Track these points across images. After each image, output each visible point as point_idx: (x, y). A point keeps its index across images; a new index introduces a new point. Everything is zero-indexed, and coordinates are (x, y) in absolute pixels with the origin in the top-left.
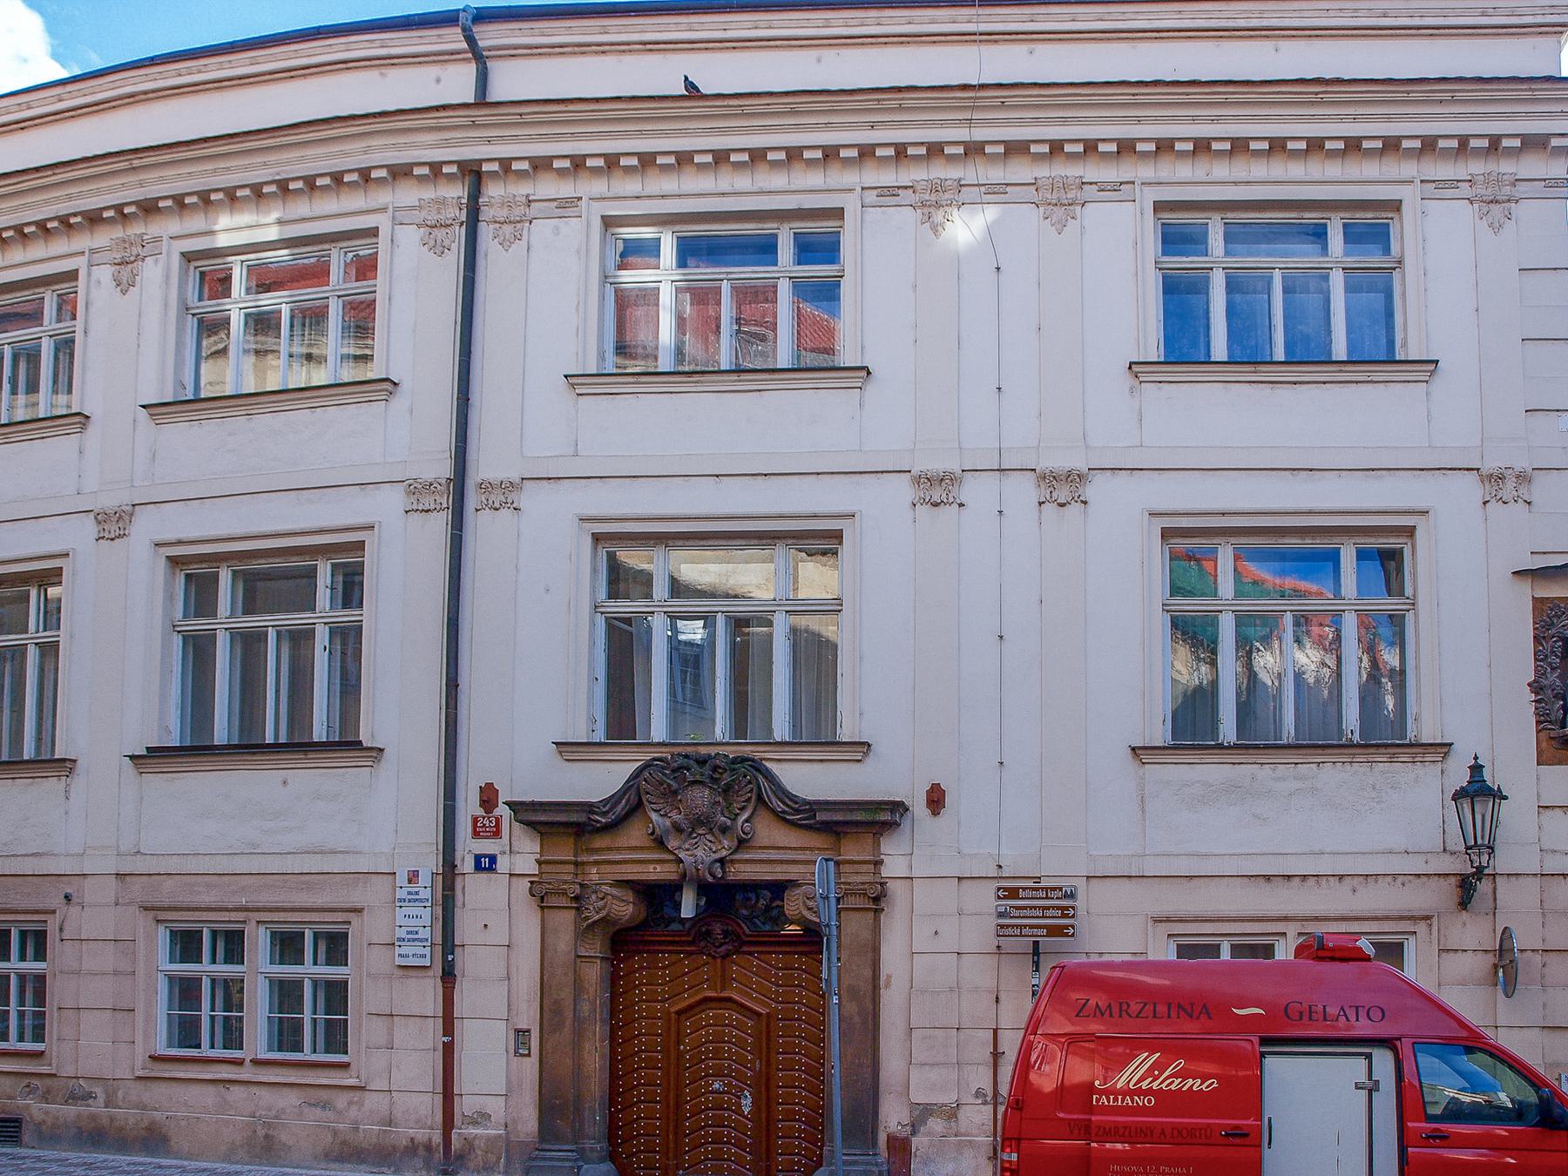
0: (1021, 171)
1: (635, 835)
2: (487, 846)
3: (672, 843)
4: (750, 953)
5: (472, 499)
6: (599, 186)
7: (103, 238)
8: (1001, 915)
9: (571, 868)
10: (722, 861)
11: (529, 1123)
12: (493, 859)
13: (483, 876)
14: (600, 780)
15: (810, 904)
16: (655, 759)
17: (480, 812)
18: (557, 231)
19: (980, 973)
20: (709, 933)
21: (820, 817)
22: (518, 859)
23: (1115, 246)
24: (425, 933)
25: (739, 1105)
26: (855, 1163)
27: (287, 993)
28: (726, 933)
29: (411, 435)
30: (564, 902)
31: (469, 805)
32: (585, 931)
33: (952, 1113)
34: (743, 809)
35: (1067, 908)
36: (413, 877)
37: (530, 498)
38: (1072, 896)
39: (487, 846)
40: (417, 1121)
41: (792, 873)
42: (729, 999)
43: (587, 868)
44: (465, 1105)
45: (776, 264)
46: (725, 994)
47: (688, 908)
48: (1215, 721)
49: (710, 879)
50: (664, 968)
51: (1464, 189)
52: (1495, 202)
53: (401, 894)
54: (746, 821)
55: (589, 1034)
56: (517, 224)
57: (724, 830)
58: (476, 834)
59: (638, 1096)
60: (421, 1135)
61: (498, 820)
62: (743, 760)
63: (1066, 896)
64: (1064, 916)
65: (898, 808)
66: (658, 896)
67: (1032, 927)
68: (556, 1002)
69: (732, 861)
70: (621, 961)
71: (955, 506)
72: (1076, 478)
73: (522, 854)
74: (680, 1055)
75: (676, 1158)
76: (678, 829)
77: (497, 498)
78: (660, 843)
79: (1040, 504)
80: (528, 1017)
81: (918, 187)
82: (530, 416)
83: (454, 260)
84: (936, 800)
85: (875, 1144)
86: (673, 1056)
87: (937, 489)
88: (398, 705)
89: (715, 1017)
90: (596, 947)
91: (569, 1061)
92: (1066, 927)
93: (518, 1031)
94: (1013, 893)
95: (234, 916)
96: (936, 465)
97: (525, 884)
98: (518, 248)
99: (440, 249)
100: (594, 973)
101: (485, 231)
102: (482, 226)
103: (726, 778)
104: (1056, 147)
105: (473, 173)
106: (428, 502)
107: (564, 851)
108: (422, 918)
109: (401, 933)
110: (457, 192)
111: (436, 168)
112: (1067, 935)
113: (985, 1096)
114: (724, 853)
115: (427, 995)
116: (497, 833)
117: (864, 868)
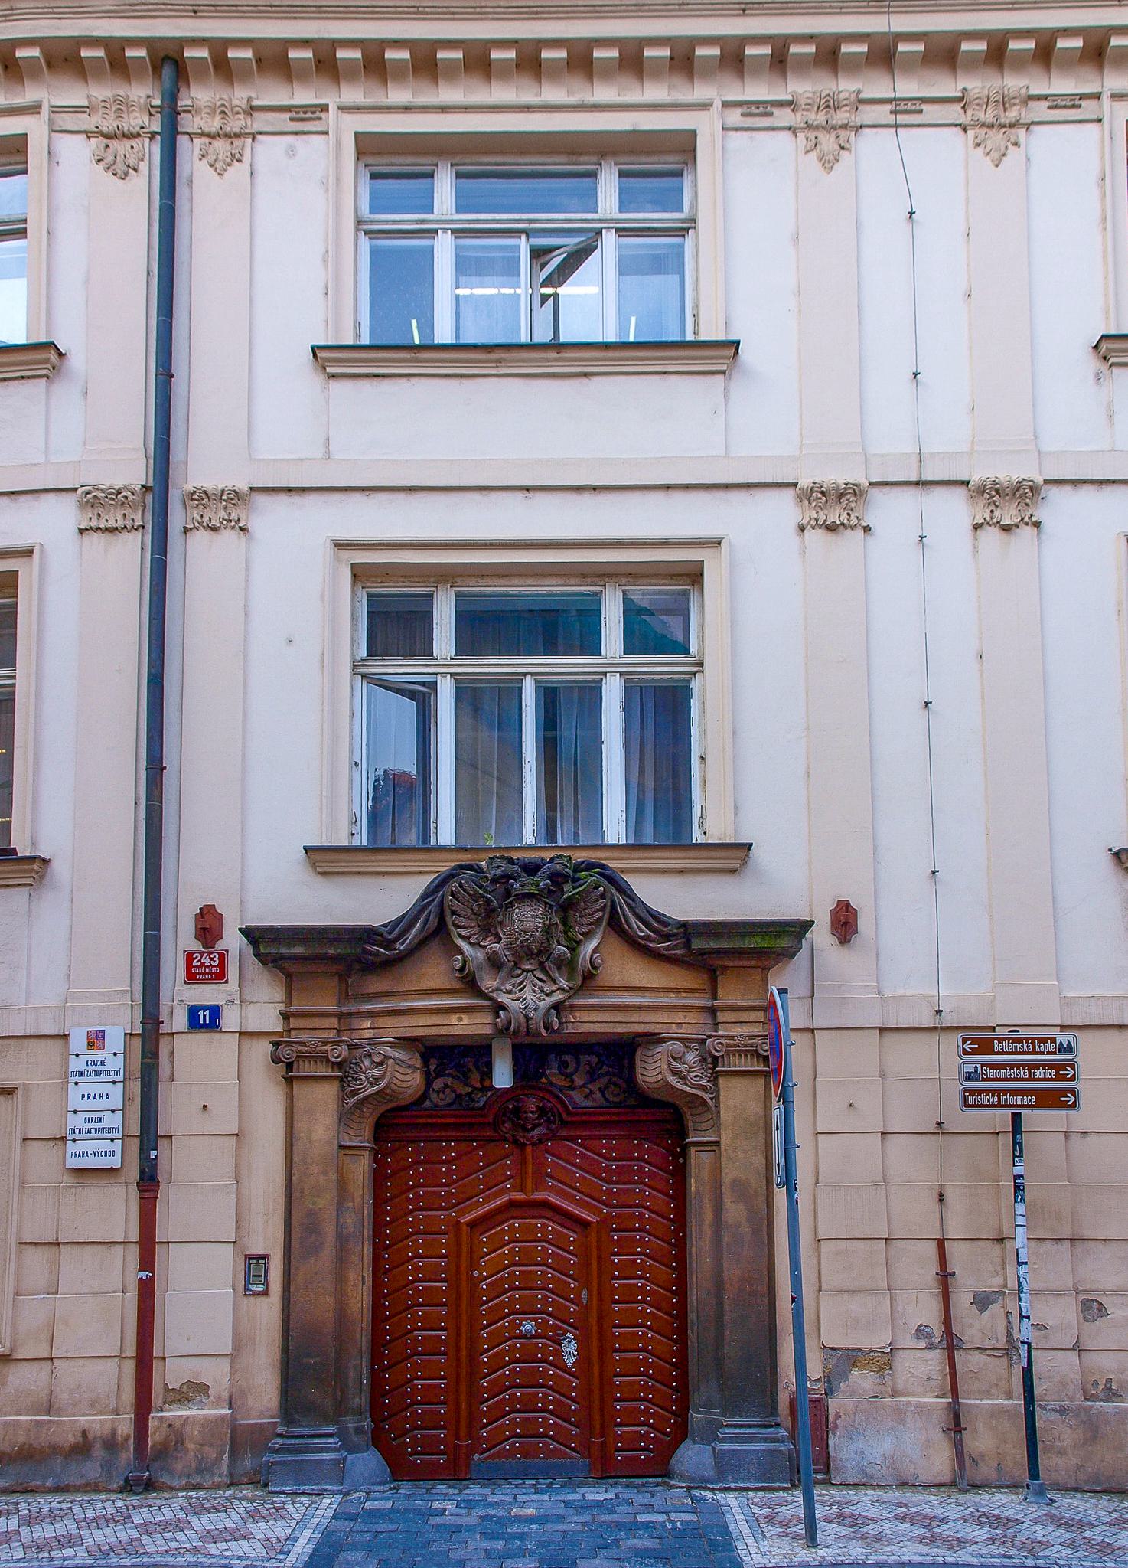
1: (434, 972)
2: (206, 994)
3: (488, 983)
4: (573, 1139)
5: (177, 518)
8: (969, 1077)
9: (334, 1022)
10: (556, 1006)
11: (264, 1395)
12: (215, 1012)
13: (201, 1038)
14: (383, 900)
16: (461, 867)
17: (196, 947)
18: (291, 152)
19: (912, 1165)
20: (517, 1111)
21: (697, 944)
22: (251, 1011)
24: (116, 1120)
25: (559, 1354)
26: (751, 1439)
28: (542, 1111)
30: (322, 1070)
33: (882, 1360)
34: (588, 935)
35: (1063, 1067)
36: (96, 1040)
37: (271, 520)
39: (206, 994)
40: (92, 1405)
41: (652, 1022)
42: (546, 1204)
43: (356, 1023)
44: (172, 1374)
46: (539, 1196)
47: (502, 1077)
53: (75, 1065)
54: (594, 951)
55: (355, 1258)
58: (191, 978)
60: (98, 1423)
61: (223, 957)
62: (590, 866)
63: (1061, 1049)
64: (1064, 1078)
65: (805, 926)
67: (1014, 1093)
68: (310, 1213)
69: (572, 1006)
70: (386, 1155)
71: (860, 532)
72: (1026, 493)
73: (256, 1004)
74: (474, 1283)
75: (469, 1435)
76: (495, 963)
78: (469, 983)
79: (977, 527)
80: (267, 1238)
81: (802, 102)
82: (261, 408)
84: (845, 922)
85: (773, 1410)
86: (464, 1287)
87: (835, 508)
89: (523, 1229)
90: (362, 1136)
91: (329, 1300)
92: (1064, 1093)
93: (249, 1258)
94: (982, 1044)
96: (836, 476)
97: (265, 1047)
98: (238, 172)
99: (123, 172)
100: (361, 1169)
101: (189, 151)
102: (182, 141)
103: (569, 891)
106: (114, 518)
108: (100, 1101)
109: (76, 1121)
112: (1065, 1105)
113: (930, 1336)
114: (558, 996)
115: (114, 1211)
116: (220, 976)
117: (752, 1016)
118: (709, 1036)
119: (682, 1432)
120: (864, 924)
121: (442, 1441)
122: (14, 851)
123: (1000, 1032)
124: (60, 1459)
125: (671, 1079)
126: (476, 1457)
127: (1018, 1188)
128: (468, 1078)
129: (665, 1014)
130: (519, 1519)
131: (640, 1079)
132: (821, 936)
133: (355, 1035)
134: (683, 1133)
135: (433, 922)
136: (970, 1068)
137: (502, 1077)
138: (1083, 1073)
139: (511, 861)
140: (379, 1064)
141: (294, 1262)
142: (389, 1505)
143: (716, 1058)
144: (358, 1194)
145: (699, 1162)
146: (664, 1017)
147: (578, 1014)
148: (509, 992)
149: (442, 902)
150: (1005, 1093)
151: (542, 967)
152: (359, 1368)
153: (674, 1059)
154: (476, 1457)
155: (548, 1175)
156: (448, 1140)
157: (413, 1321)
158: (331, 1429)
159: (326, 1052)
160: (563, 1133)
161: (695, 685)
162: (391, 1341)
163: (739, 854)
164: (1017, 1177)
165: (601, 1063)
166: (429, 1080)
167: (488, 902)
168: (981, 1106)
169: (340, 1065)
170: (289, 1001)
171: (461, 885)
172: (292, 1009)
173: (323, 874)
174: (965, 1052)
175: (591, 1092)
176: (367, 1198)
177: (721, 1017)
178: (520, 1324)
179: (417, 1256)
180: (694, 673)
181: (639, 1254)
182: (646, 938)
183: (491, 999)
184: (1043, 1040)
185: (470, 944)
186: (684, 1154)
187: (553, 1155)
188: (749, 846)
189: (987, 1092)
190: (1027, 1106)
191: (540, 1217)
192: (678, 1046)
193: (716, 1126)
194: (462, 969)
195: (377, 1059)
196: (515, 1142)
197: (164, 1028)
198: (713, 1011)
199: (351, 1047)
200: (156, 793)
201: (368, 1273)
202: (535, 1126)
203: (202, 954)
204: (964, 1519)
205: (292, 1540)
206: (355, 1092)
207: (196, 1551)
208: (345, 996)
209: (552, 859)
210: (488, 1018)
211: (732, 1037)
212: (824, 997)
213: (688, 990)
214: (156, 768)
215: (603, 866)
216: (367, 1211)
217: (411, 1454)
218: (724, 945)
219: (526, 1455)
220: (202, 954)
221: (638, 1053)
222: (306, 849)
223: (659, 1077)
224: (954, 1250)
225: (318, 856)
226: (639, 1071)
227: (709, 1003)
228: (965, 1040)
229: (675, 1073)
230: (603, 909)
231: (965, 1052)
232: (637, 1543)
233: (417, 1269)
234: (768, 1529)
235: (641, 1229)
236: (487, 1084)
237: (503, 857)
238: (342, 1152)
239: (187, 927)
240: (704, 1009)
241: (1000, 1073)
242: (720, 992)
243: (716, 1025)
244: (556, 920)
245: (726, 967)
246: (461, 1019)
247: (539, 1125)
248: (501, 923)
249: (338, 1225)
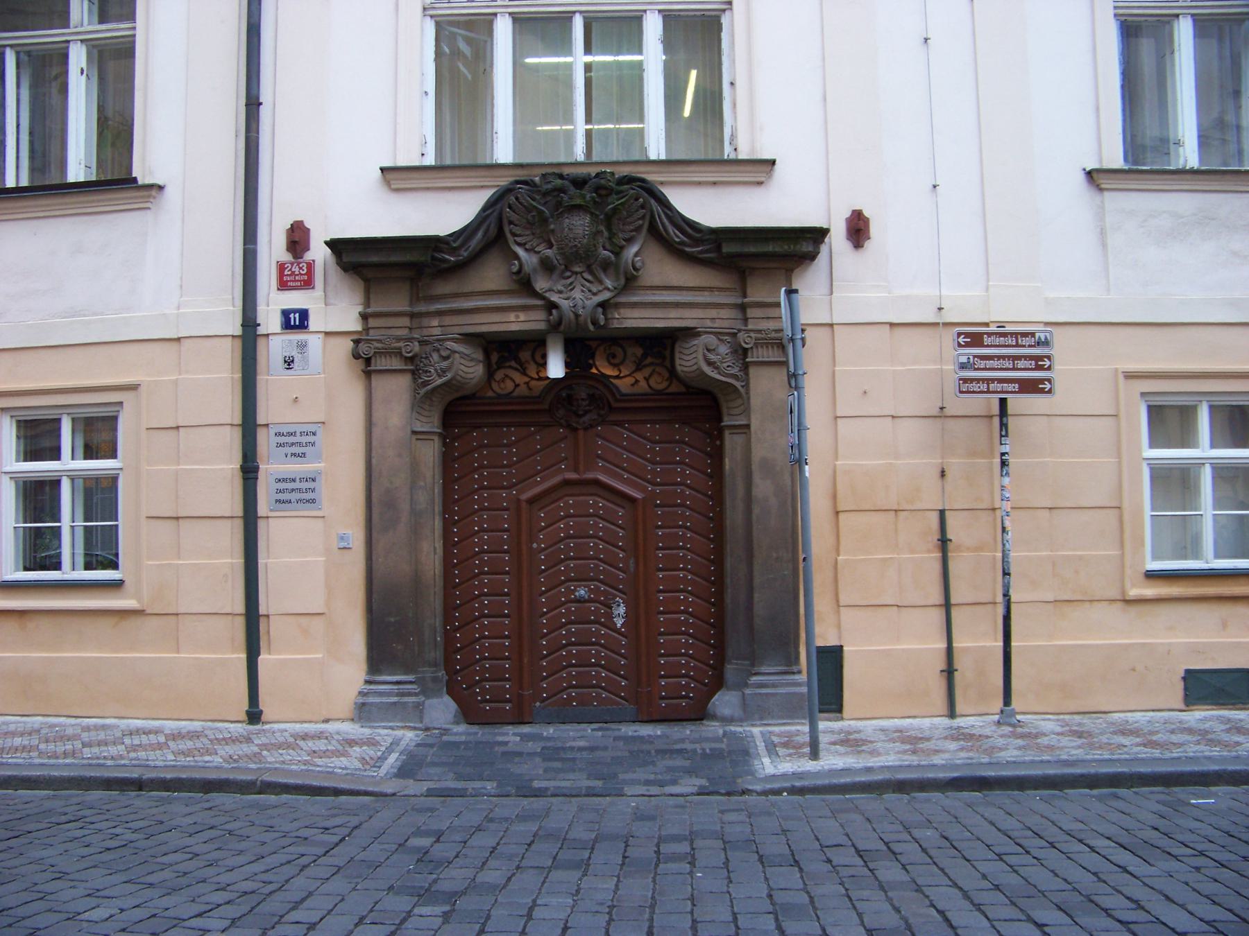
1: (492, 275)
2: (295, 300)
3: (541, 284)
8: (963, 366)
9: (405, 321)
10: (603, 305)
12: (304, 314)
14: (447, 214)
15: (712, 357)
16: (518, 182)
17: (287, 257)
21: (727, 249)
25: (610, 616)
28: (592, 397)
30: (396, 364)
31: (272, 249)
32: (422, 399)
34: (630, 241)
35: (1041, 358)
38: (1046, 343)
39: (295, 300)
42: (597, 483)
45: (68, 27)
49: (591, 328)
50: (509, 446)
54: (636, 255)
57: (606, 266)
58: (283, 285)
59: (480, 609)
61: (310, 266)
62: (630, 180)
63: (1039, 344)
64: (1039, 368)
65: (818, 235)
66: (507, 351)
67: (1001, 381)
70: (454, 440)
73: (336, 310)
76: (547, 266)
78: (524, 284)
84: (858, 229)
88: (180, 128)
90: (432, 423)
92: (1042, 381)
94: (975, 339)
97: (348, 344)
100: (430, 453)
107: (397, 301)
112: (1042, 391)
114: (606, 295)
116: (308, 283)
118: (739, 331)
119: (718, 683)
120: (874, 229)
121: (507, 691)
122: (135, 180)
123: (993, 328)
125: (708, 370)
126: (538, 704)
127: (1004, 464)
128: (524, 369)
129: (700, 311)
130: (572, 748)
131: (679, 368)
132: (838, 237)
133: (426, 332)
134: (720, 420)
135: (493, 231)
136: (963, 359)
137: (556, 368)
138: (1057, 367)
139: (561, 176)
140: (446, 358)
141: (375, 535)
143: (745, 351)
144: (429, 474)
145: (732, 442)
146: (699, 313)
147: (622, 311)
148: (560, 292)
149: (500, 214)
150: (993, 380)
151: (589, 269)
152: (432, 617)
153: (708, 350)
154: (538, 704)
155: (599, 456)
156: (509, 425)
157: (480, 652)
158: (410, 678)
159: (400, 348)
160: (613, 417)
161: (725, 20)
162: (461, 605)
163: (766, 168)
164: (1003, 454)
165: (645, 356)
166: (490, 373)
167: (540, 212)
168: (974, 392)
169: (411, 360)
170: (367, 303)
171: (517, 199)
172: (369, 310)
173: (397, 190)
174: (960, 345)
175: (637, 381)
176: (437, 477)
177: (751, 313)
178: (575, 590)
179: (483, 530)
180: (724, 11)
181: (680, 527)
182: (682, 243)
183: (544, 298)
184: (1025, 335)
185: (526, 250)
186: (720, 437)
187: (604, 439)
188: (773, 162)
189: (978, 380)
190: (1012, 392)
191: (591, 495)
192: (711, 340)
193: (747, 411)
194: (519, 272)
195: (444, 354)
196: (569, 426)
197: (261, 330)
198: (743, 308)
199: (422, 343)
200: (254, 126)
201: (439, 545)
202: (586, 412)
203: (292, 264)
204: (946, 738)
205: (383, 759)
206: (425, 384)
207: (306, 763)
208: (415, 298)
209: (598, 175)
210: (541, 315)
211: (759, 331)
212: (828, 297)
213: (720, 289)
214: (253, 104)
215: (643, 180)
216: (438, 490)
217: (481, 702)
218: (752, 249)
219: (581, 703)
220: (292, 264)
221: (677, 346)
222: (382, 169)
223: (695, 367)
224: (951, 520)
225: (390, 176)
226: (678, 362)
227: (739, 301)
228: (959, 334)
229: (710, 363)
230: (643, 218)
231: (960, 345)
232: (670, 763)
233: (484, 669)
234: (781, 751)
235: (682, 505)
236: (542, 375)
237: (554, 174)
238: (414, 437)
239: (280, 241)
240: (735, 306)
241: (990, 363)
242: (749, 291)
243: (746, 320)
244: (602, 228)
245: (754, 269)
246: (517, 317)
247: (590, 411)
248: (553, 231)
249: (412, 501)
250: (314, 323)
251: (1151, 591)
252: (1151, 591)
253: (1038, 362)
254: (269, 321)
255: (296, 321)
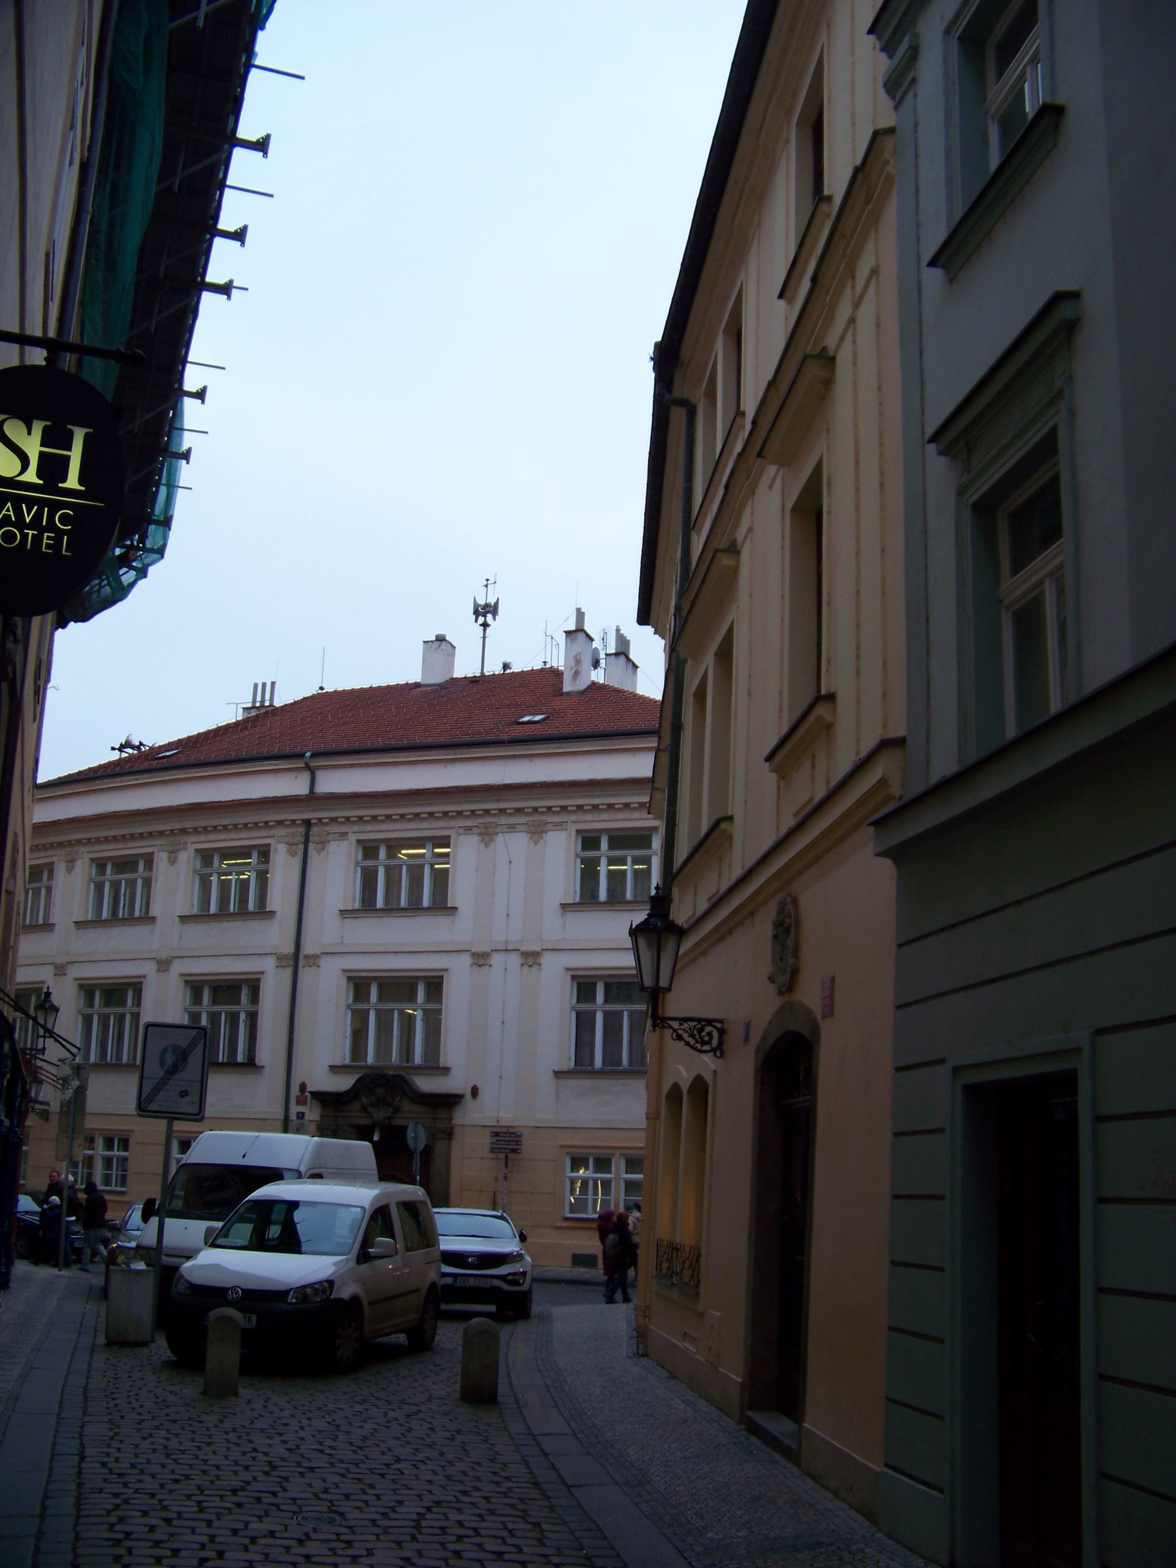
0: (522, 819)
1: (356, 1106)
2: (301, 1109)
3: (370, 1109)
5: (301, 962)
6: (356, 828)
7: (63, 852)
12: (303, 1114)
14: (344, 1083)
23: (559, 853)
27: (108, 1162)
29: (276, 935)
37: (325, 962)
48: (592, 1059)
51: (475, 830)
52: (487, 836)
56: (323, 844)
77: (311, 961)
82: (325, 928)
83: (298, 859)
84: (475, 1091)
87: (481, 959)
88: (269, 1050)
94: (497, 1134)
95: (583, 1151)
101: (311, 846)
104: (535, 809)
105: (308, 823)
106: (285, 963)
110: (302, 830)
111: (293, 821)
116: (305, 1103)
124: (538, 1535)
142: (9, 1062)
212: (469, 1115)
239: (297, 1088)
250: (306, 1117)
251: (564, 1224)
252: (564, 1224)
253: (517, 1143)
254: (293, 1116)
255: (301, 1116)
